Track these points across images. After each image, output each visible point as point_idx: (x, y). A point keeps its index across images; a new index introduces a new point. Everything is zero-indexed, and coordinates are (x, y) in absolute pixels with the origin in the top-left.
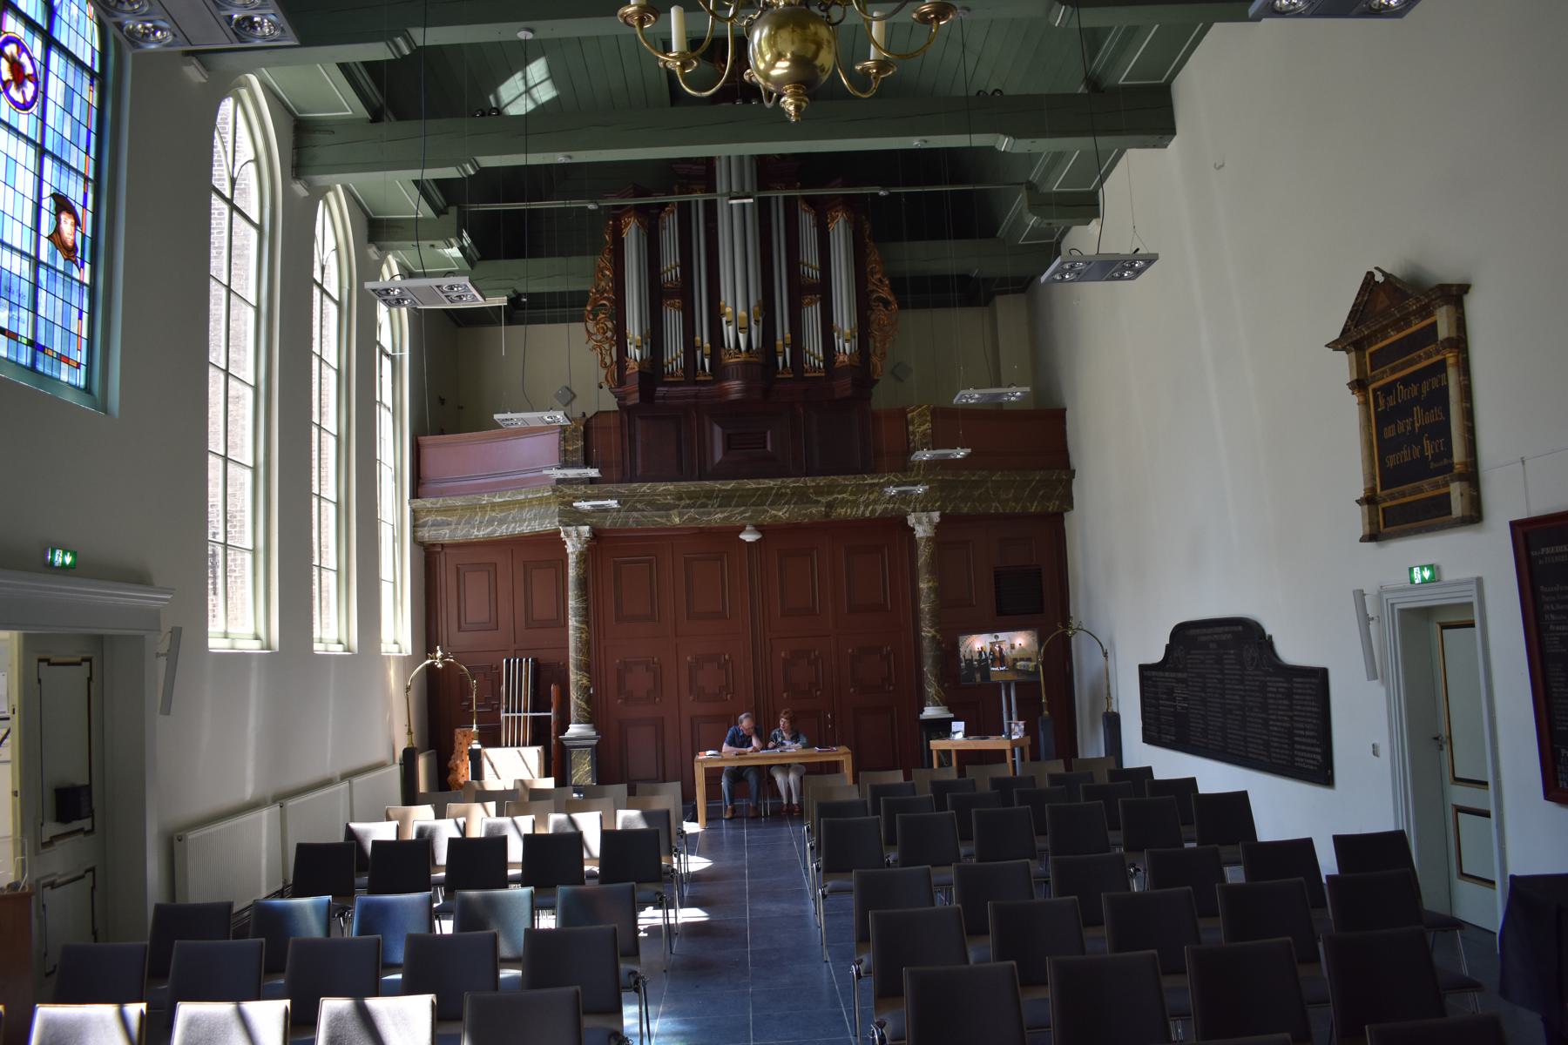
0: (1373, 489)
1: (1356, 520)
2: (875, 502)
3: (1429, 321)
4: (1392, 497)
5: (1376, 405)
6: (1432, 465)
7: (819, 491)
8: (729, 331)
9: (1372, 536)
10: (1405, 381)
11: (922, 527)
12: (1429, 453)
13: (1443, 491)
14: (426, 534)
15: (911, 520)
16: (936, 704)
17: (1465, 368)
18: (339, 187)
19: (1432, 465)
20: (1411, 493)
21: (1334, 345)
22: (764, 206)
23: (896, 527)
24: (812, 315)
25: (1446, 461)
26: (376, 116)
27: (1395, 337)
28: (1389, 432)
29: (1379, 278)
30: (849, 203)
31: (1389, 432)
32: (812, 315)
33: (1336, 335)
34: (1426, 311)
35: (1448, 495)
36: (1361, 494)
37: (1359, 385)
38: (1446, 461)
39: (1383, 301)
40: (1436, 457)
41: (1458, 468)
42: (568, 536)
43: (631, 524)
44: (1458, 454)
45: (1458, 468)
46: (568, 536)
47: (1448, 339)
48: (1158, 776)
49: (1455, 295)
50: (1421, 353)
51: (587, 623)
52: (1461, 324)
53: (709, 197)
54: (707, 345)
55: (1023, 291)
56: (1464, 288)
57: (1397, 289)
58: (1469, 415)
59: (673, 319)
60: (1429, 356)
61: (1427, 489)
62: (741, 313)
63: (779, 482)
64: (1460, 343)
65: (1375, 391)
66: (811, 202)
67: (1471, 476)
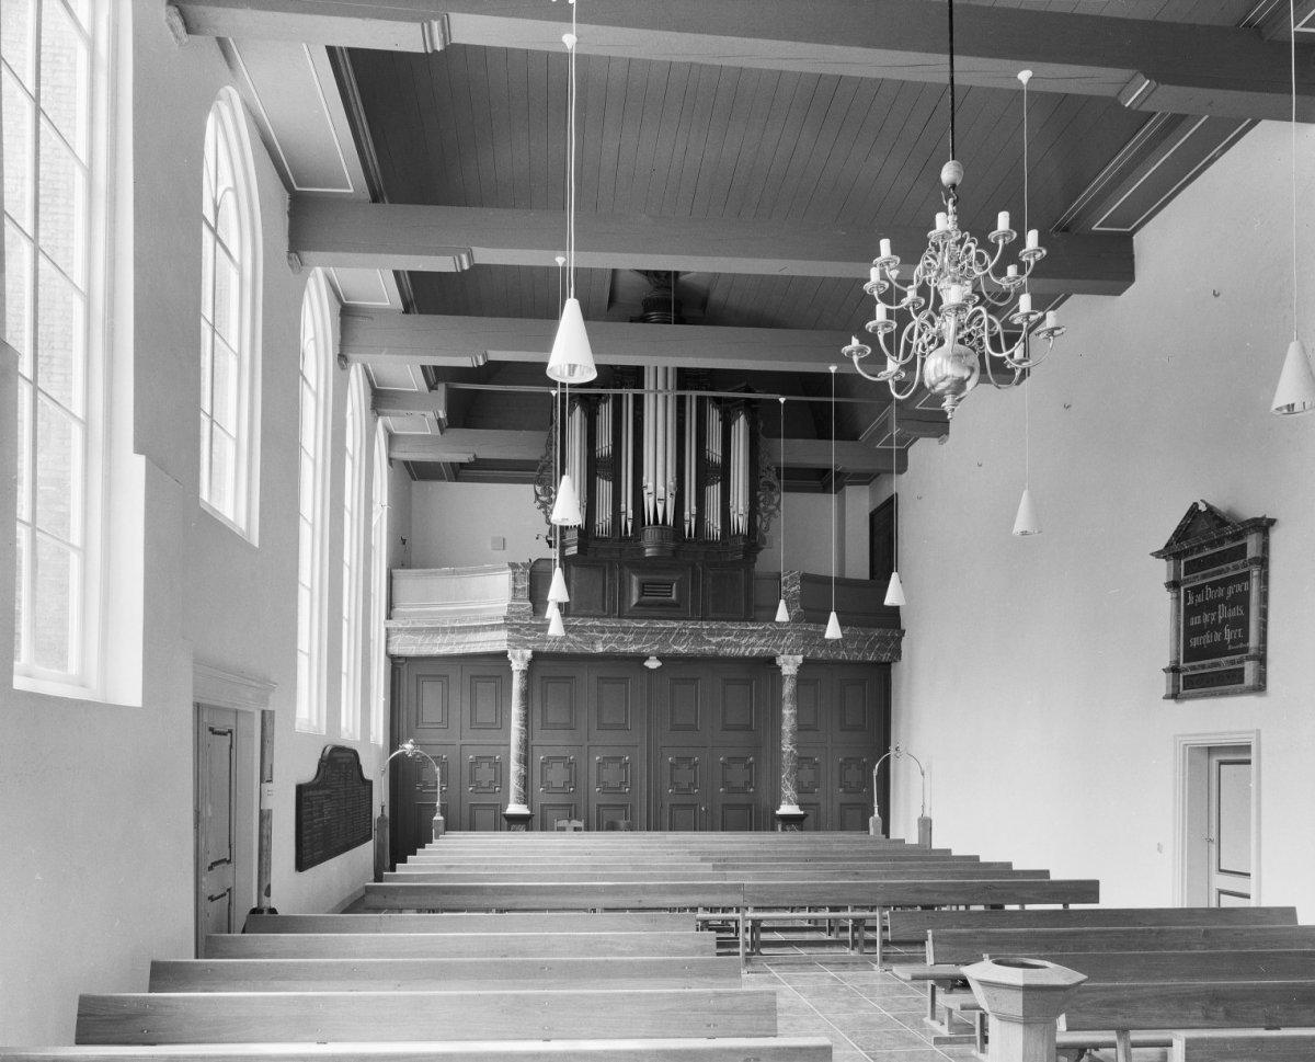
0: (1178, 662)
1: (1163, 683)
2: (753, 645)
3: (1239, 543)
4: (1193, 668)
5: (1186, 600)
6: (1230, 647)
7: (711, 633)
8: (649, 501)
9: (1175, 696)
10: (1214, 585)
11: (789, 665)
12: (1228, 638)
13: (1238, 666)
14: (396, 650)
15: (780, 661)
16: (790, 803)
17: (1265, 579)
18: (359, 365)
19: (1230, 647)
20: (1206, 666)
21: (1158, 555)
22: (681, 401)
23: (769, 663)
24: (714, 492)
25: (1241, 645)
26: (407, 311)
27: (1208, 552)
28: (1195, 621)
29: (1202, 508)
30: (750, 407)
31: (1195, 621)
32: (714, 492)
33: (1161, 546)
34: (1239, 536)
35: (1242, 669)
36: (1167, 664)
37: (1173, 585)
38: (1241, 645)
39: (1203, 525)
40: (1233, 642)
41: (1252, 652)
42: (514, 657)
43: (564, 650)
44: (1253, 642)
45: (1252, 652)
46: (514, 657)
47: (1255, 558)
48: (982, 860)
49: (1263, 526)
50: (1230, 565)
51: (526, 726)
52: (1265, 547)
53: (638, 391)
54: (630, 512)
55: (868, 484)
56: (1272, 522)
57: (1216, 517)
58: (1264, 613)
59: (604, 488)
60: (1236, 568)
61: (1224, 663)
62: (661, 488)
63: (682, 623)
64: (1263, 562)
65: (1186, 590)
66: (718, 401)
67: (1261, 659)
